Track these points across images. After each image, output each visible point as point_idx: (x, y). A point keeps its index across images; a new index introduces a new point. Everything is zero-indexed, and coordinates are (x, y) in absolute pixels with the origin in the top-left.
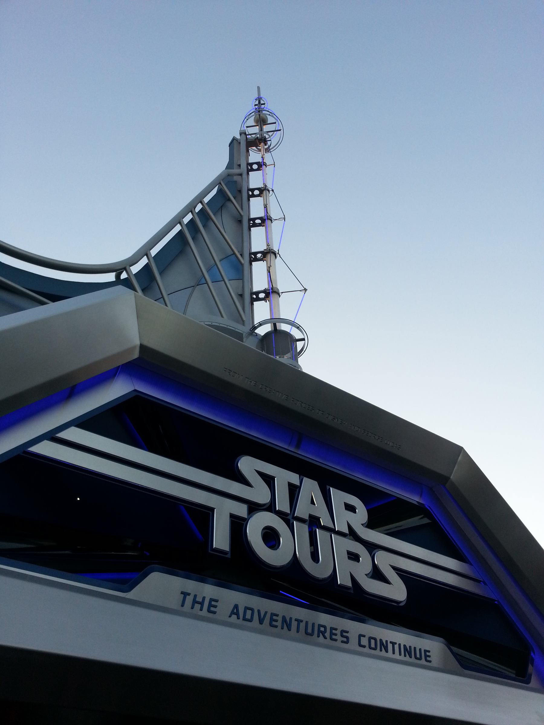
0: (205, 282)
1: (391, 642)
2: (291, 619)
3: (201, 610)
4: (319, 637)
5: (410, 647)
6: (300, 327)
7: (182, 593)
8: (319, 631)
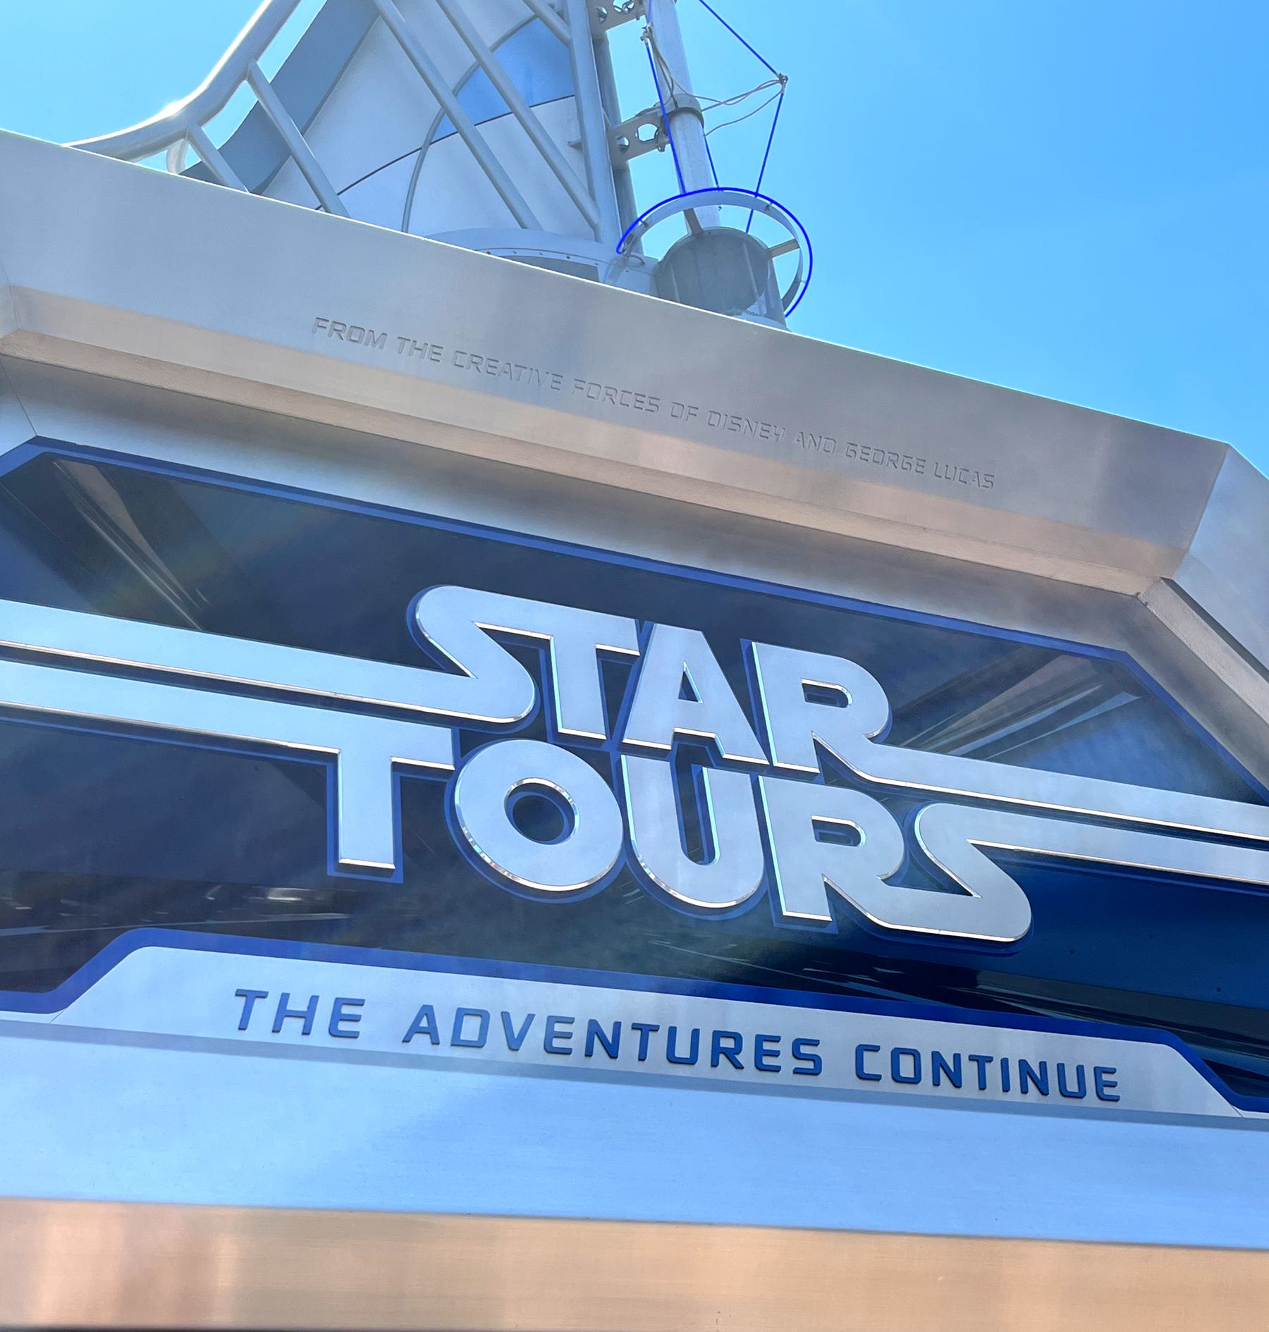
0: (456, 130)
1: (972, 1058)
2: (957, 1057)
3: (306, 1032)
4: (716, 1066)
5: (1043, 1065)
6: (773, 205)
7: (239, 993)
8: (717, 1051)
